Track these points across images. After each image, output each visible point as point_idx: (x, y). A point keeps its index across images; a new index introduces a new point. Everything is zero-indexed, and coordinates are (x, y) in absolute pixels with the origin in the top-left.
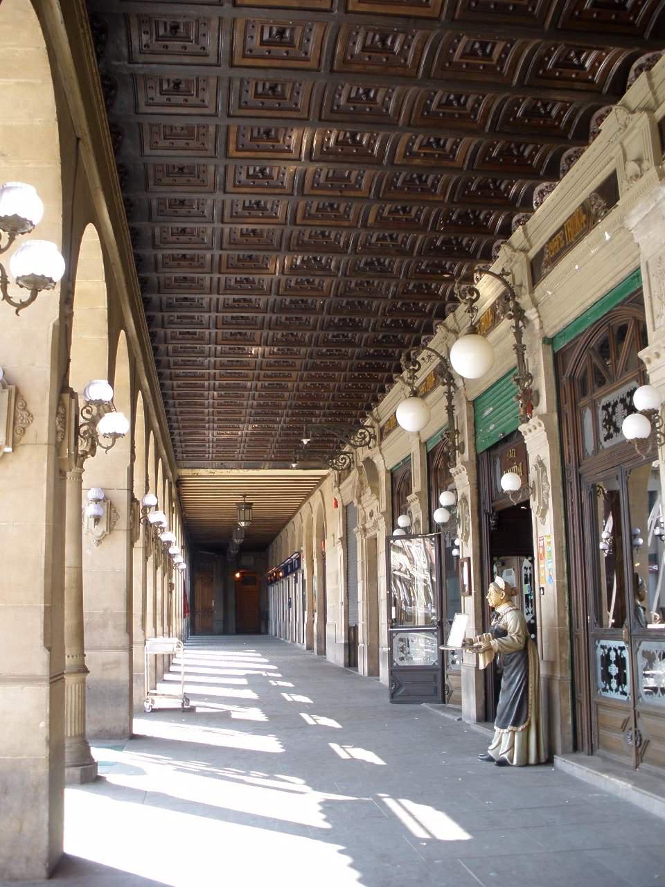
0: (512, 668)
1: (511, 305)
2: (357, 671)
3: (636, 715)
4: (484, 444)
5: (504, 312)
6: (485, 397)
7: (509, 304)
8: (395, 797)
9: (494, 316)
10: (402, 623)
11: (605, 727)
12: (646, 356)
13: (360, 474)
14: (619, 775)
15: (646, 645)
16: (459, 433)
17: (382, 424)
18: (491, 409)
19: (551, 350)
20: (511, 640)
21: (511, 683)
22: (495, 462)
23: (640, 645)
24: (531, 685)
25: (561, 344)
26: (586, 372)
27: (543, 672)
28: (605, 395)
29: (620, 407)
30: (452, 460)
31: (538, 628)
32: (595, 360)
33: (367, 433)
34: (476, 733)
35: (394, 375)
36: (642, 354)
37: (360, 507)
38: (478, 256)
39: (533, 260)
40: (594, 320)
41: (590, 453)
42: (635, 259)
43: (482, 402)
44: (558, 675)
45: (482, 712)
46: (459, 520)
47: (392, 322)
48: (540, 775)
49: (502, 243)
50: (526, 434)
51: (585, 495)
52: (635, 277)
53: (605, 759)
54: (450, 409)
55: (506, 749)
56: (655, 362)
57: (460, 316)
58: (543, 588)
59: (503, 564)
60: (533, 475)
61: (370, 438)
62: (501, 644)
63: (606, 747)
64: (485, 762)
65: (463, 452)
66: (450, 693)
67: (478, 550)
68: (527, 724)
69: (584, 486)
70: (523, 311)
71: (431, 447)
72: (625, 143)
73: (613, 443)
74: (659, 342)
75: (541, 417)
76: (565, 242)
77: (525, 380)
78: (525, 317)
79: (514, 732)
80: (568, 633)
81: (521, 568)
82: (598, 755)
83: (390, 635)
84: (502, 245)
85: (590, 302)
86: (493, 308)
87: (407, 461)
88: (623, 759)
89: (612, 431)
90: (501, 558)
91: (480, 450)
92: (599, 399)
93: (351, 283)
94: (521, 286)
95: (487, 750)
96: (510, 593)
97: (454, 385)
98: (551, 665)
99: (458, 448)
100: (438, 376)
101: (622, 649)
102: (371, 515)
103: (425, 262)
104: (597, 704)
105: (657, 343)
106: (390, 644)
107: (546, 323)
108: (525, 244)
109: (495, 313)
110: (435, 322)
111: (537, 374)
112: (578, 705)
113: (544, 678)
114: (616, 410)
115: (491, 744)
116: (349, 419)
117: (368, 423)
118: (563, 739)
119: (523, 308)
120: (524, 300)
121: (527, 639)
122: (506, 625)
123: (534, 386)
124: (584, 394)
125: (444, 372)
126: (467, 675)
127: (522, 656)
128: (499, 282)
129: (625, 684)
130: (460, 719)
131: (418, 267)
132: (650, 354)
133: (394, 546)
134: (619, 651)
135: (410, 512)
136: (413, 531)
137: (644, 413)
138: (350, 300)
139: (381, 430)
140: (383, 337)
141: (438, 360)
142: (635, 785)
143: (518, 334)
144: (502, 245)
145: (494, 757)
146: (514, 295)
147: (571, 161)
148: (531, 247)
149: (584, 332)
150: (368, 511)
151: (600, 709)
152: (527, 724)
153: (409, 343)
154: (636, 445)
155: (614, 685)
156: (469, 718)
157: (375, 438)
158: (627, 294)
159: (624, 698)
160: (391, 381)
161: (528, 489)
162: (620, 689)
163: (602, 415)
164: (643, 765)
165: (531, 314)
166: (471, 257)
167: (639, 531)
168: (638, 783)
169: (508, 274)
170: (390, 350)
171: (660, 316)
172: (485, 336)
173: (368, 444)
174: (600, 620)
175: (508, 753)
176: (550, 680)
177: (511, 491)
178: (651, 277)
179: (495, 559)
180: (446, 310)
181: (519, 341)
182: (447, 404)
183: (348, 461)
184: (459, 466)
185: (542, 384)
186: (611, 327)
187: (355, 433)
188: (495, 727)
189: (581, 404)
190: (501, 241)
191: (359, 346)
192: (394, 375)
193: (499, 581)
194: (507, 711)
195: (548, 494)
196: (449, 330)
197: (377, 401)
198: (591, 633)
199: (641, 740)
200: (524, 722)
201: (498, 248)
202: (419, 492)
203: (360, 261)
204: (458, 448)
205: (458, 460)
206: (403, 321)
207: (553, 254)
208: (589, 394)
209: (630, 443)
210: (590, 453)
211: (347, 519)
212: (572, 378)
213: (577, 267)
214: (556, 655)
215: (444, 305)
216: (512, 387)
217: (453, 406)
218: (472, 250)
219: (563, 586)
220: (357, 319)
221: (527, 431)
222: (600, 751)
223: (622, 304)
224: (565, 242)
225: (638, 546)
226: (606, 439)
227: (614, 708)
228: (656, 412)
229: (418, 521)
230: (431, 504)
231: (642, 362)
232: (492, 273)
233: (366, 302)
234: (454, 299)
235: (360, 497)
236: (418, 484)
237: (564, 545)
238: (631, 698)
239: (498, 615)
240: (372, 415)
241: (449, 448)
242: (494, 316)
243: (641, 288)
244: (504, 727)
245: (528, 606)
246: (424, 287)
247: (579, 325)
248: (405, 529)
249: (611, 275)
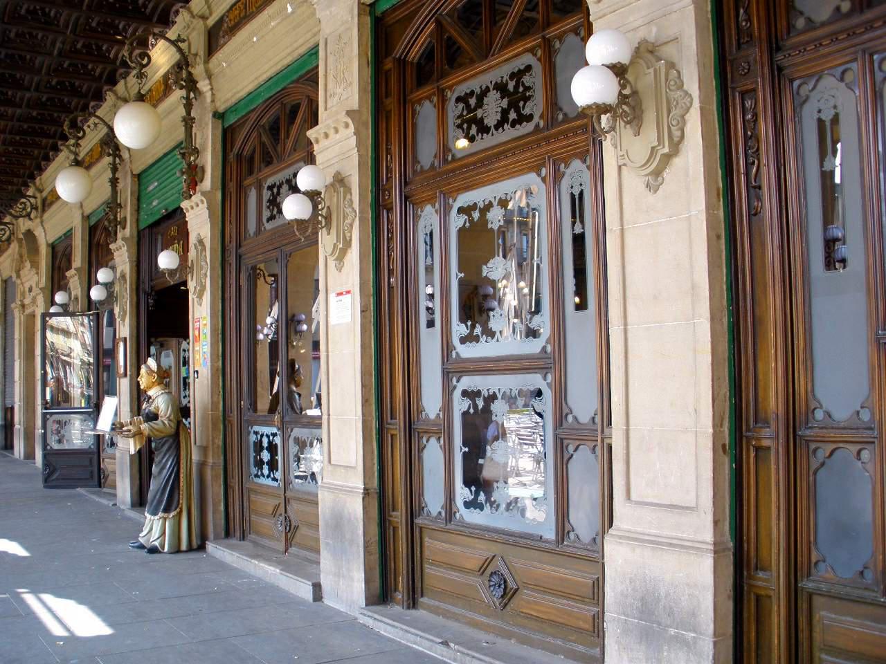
0: (162, 454)
1: (184, 74)
2: (13, 454)
3: (286, 501)
4: (146, 220)
5: (176, 82)
6: (151, 170)
7: (183, 75)
8: (35, 591)
9: (166, 87)
10: (59, 404)
11: (257, 513)
12: (314, 136)
13: (20, 247)
14: (268, 560)
15: (298, 432)
16: (121, 207)
17: (45, 194)
18: (156, 184)
19: (221, 126)
20: (161, 423)
21: (163, 469)
22: (156, 239)
23: (291, 431)
24: (183, 471)
25: (232, 119)
26: (254, 151)
27: (195, 457)
29: (285, 187)
30: (112, 234)
31: (192, 412)
32: (264, 139)
33: (28, 204)
34: (129, 519)
35: (60, 143)
36: (311, 134)
37: (19, 281)
38: (155, 19)
39: (211, 28)
40: (268, 96)
41: (252, 235)
42: (315, 35)
43: (147, 176)
44: (210, 460)
45: (136, 497)
46: (116, 298)
47: (58, 83)
48: (190, 562)
49: (181, 7)
50: (188, 211)
51: (244, 276)
52: (313, 54)
53: (255, 544)
54: (114, 182)
55: (156, 537)
56: (324, 143)
57: (129, 85)
58: (197, 372)
59: (162, 345)
60: (192, 254)
61: (31, 209)
62: (152, 429)
63: (257, 533)
64: (136, 550)
65: (124, 228)
66: (106, 478)
67: (135, 331)
68: (178, 510)
69: (243, 268)
70: (195, 82)
71: (93, 221)
73: (276, 225)
74: (329, 122)
75: (203, 194)
76: (246, 12)
77: (190, 154)
78: (198, 89)
79: (165, 519)
80: (221, 418)
81: (179, 349)
82: (250, 541)
83: (44, 415)
84: (181, 10)
85: (265, 77)
86: (166, 77)
88: (272, 544)
89: (275, 212)
90: (159, 340)
91: (142, 226)
93: (10, 32)
94: (196, 55)
95: (138, 536)
96: (163, 377)
97: (120, 157)
98: (204, 450)
99: (120, 223)
100: (104, 147)
101: (274, 435)
102: (30, 290)
103: (96, 19)
104: (249, 490)
105: (328, 122)
106: (44, 426)
107: (218, 95)
108: (205, 11)
109: (167, 82)
110: (106, 88)
111: (205, 149)
112: (230, 491)
113: (197, 463)
114: (281, 190)
115: (142, 531)
116: (10, 187)
117: (30, 193)
118: (215, 525)
119: (195, 79)
120: (198, 70)
121: (179, 423)
122: (157, 408)
123: (199, 162)
124: (251, 172)
125: (110, 143)
126: (122, 458)
127: (174, 441)
128: (174, 49)
129: (277, 470)
130: (115, 505)
131: (88, 24)
132: (319, 134)
133: (52, 328)
134: (271, 438)
135: (69, 289)
136: (71, 309)
137: (307, 194)
138: (10, 52)
139: (44, 201)
140: (48, 99)
141: (105, 130)
142: (281, 570)
143: (188, 106)
144: (181, 10)
145: (145, 545)
146: (187, 65)
148: (211, 14)
149: (255, 109)
150: (27, 286)
151: (252, 496)
152: (178, 510)
153: (76, 108)
154: (295, 227)
155: (266, 471)
156: (124, 503)
157: (36, 209)
158: (303, 71)
159: (276, 484)
160: (56, 150)
161: (186, 268)
162: (272, 476)
163: (267, 195)
164: (293, 550)
165: (203, 85)
166: (147, 19)
167: (304, 317)
168: (286, 567)
169: (184, 41)
170: (56, 115)
171: (333, 95)
172: (155, 106)
173: (28, 215)
174: (254, 406)
175: (159, 540)
176: (202, 465)
177: (168, 270)
178: (328, 54)
179: (153, 340)
180: (118, 75)
181: (189, 113)
182: (111, 176)
183: (8, 233)
184: (120, 242)
185: (209, 160)
186: (284, 105)
187: (16, 201)
188: (146, 514)
190: (180, 4)
191: (20, 107)
192: (60, 143)
193: (152, 362)
194: (157, 497)
195: (206, 274)
196: (118, 98)
197: (41, 170)
198: (244, 418)
199: (290, 526)
200: (176, 509)
201: (177, 12)
202: (79, 268)
203: (21, 7)
204: (120, 223)
205: (119, 235)
206: (70, 82)
207: (232, 22)
208: (254, 175)
209: (289, 223)
210: (252, 235)
211: (5, 295)
212: (239, 157)
213: (255, 39)
214: (208, 441)
215: (115, 71)
216: (178, 162)
217: (118, 179)
218: (148, 11)
219: (217, 370)
220: (18, 76)
221: (189, 208)
222: (252, 536)
223: (297, 81)
224: (246, 12)
225: (301, 332)
226: (268, 220)
227: (266, 494)
228: (319, 193)
229: (76, 299)
230: (91, 281)
231: (309, 140)
232: (168, 40)
233: (28, 57)
234: (124, 64)
235: (19, 271)
236: (78, 260)
237: (220, 327)
238: (282, 485)
239: (150, 398)
240: (35, 184)
241: (110, 222)
242: (166, 89)
243: (317, 67)
244: (154, 513)
245: (185, 390)
246: (94, 47)
247: (252, 101)
248: (61, 305)
249: (288, 51)
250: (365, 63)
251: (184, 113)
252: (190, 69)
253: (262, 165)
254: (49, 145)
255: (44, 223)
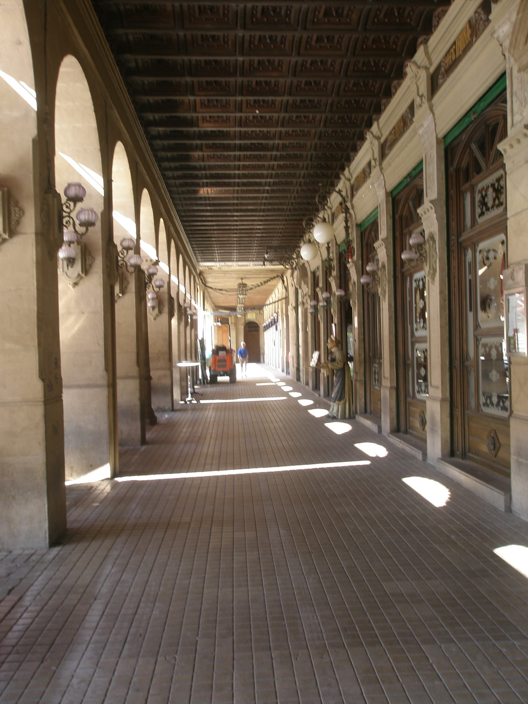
28: (480, 181)
72: (418, 84)
79: (339, 404)
87: (417, 172)
92: (477, 184)
147: (440, 18)
163: (478, 197)
189: (463, 188)
236: (384, 232)
244: (334, 402)
250: (389, 217)
251: (345, 225)
252: (346, 204)
253: (475, 174)
254: (357, 133)
255: (383, 171)
